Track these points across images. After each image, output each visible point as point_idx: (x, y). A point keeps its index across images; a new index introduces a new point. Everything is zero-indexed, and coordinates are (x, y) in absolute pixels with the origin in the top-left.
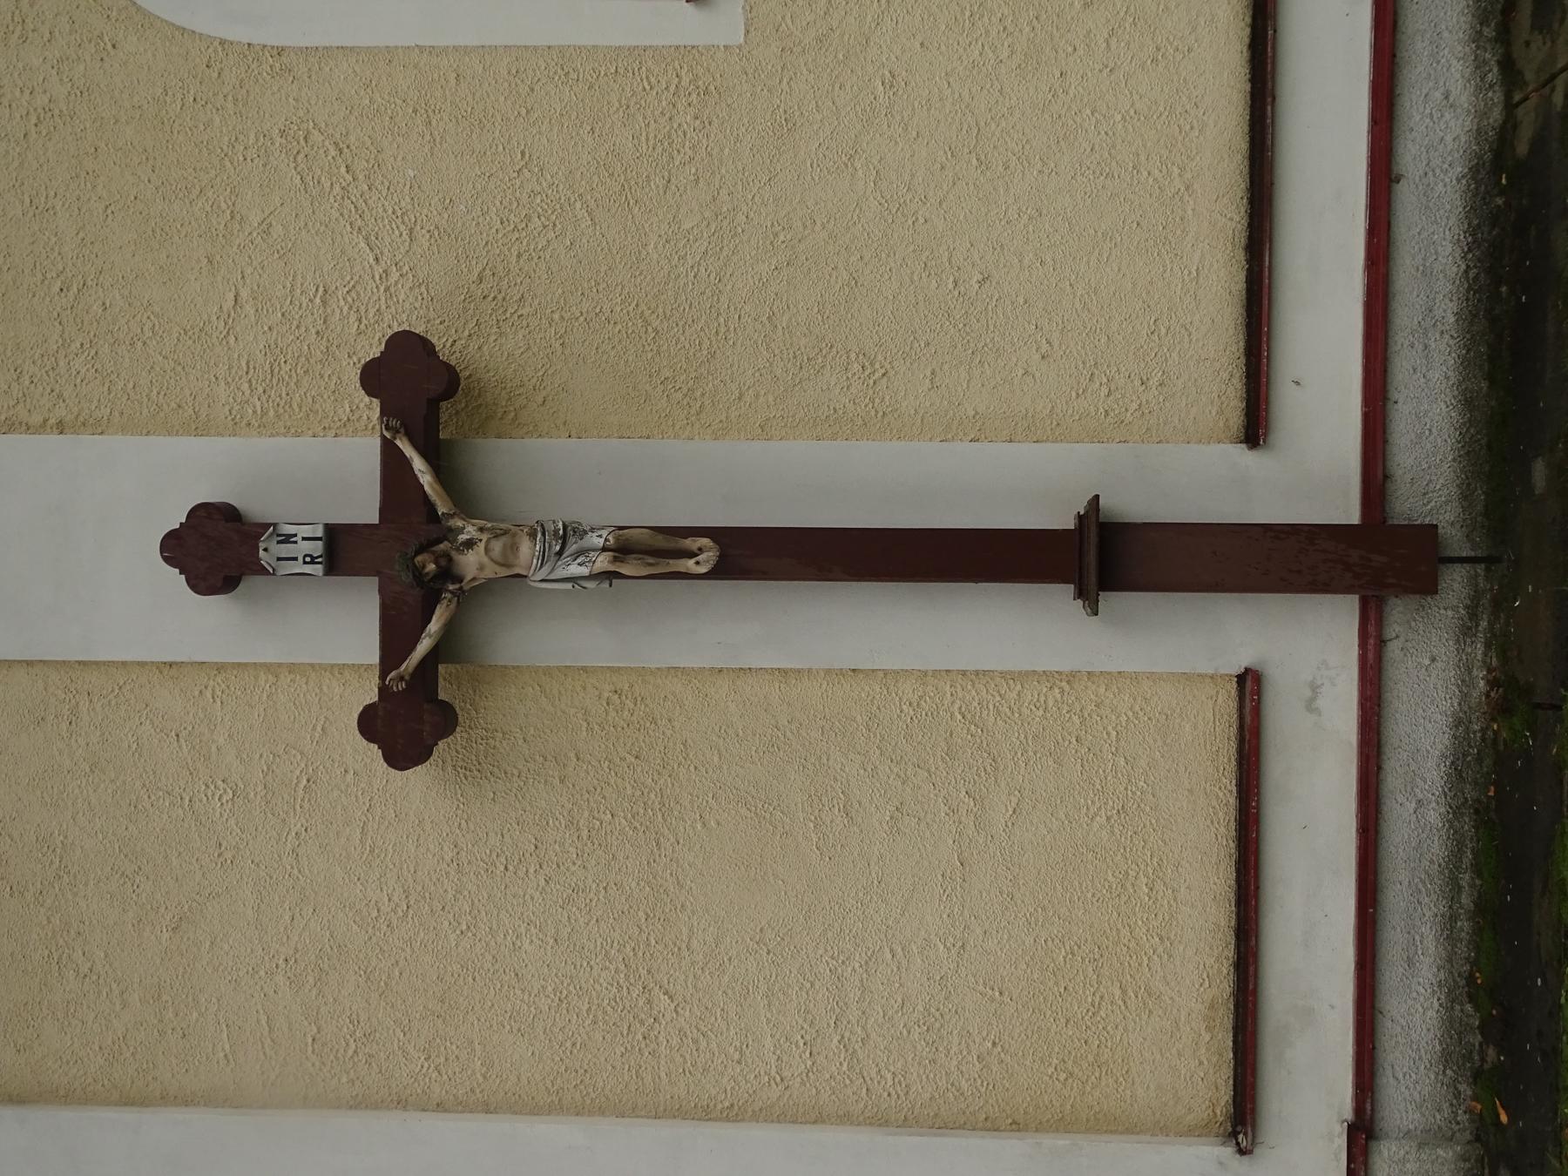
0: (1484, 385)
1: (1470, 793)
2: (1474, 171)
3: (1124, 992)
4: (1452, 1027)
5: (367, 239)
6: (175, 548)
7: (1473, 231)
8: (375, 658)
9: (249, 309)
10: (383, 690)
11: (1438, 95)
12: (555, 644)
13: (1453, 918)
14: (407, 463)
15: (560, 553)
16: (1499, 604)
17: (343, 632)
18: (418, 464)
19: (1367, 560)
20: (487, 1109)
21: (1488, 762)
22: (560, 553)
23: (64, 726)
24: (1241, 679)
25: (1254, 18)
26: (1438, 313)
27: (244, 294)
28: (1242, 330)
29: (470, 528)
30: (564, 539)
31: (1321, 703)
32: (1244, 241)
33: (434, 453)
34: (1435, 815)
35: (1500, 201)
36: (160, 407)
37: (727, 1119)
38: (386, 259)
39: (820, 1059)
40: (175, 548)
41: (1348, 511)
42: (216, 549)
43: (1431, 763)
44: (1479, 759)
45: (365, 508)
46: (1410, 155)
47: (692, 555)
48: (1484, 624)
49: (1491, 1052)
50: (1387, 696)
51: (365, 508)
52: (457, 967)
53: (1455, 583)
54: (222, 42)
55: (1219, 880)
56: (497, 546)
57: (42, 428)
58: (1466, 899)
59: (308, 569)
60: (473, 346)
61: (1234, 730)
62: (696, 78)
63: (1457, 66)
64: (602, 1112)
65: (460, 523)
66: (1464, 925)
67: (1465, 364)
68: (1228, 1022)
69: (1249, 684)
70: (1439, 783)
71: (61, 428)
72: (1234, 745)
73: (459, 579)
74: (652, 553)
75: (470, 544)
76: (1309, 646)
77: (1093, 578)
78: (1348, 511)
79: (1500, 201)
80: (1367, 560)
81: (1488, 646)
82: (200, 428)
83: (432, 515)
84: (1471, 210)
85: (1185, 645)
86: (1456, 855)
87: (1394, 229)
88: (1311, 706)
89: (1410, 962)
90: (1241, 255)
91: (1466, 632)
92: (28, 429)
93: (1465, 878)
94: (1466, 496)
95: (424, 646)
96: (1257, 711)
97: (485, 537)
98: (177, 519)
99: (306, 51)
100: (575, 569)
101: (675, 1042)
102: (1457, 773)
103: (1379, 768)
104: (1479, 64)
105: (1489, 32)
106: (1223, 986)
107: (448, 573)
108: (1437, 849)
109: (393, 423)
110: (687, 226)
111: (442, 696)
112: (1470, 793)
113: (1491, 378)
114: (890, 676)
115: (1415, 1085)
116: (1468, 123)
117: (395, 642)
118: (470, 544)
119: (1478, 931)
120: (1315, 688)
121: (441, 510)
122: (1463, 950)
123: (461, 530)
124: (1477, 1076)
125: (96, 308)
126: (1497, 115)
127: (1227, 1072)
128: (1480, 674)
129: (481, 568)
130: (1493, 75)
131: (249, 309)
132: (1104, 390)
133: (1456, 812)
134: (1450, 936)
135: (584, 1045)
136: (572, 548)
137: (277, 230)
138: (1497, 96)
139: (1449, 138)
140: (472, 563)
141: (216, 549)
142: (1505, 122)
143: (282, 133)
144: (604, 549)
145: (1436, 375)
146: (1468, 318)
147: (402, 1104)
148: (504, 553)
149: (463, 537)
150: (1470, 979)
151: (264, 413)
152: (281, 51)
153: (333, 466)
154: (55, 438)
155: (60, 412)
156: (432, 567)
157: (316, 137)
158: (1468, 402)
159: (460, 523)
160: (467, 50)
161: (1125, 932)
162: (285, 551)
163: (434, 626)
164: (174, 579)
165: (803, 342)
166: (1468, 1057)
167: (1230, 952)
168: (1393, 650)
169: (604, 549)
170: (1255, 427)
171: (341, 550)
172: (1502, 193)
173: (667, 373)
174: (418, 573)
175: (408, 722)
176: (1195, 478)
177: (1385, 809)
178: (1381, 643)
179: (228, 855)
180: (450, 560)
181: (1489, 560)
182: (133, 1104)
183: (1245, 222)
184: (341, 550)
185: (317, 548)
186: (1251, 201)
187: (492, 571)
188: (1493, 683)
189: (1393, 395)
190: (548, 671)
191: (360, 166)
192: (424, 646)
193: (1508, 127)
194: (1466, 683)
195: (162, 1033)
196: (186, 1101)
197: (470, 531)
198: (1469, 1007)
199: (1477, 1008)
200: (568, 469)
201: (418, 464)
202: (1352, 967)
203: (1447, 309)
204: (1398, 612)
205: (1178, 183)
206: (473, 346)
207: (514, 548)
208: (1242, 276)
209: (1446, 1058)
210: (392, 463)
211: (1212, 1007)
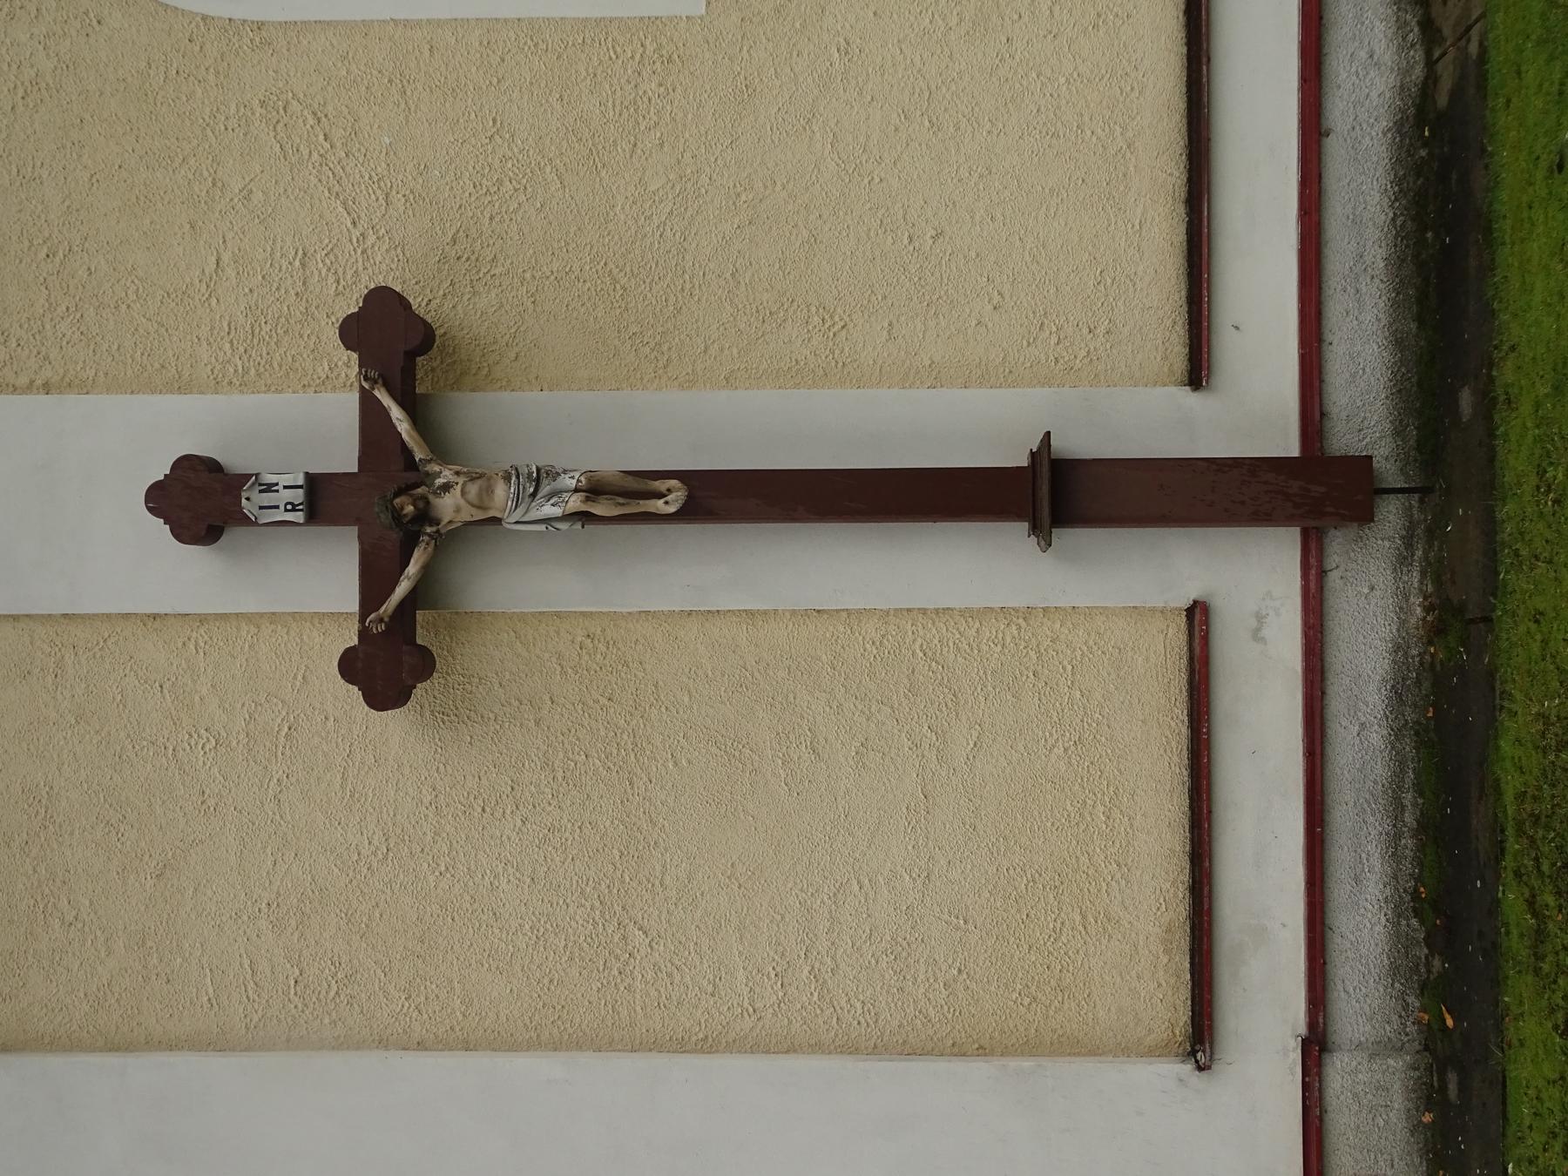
0: (1413, 326)
1: (1410, 715)
2: (1399, 126)
3: (1084, 917)
4: (1400, 942)
5: (344, 203)
6: (160, 499)
7: (1398, 181)
8: (354, 606)
11: (1363, 54)
12: (530, 589)
13: (1398, 837)
14: (385, 413)
15: (534, 495)
19: (1306, 492)
20: (467, 1046)
21: (1426, 685)
22: (534, 495)
23: (50, 679)
26: (1368, 259)
27: (226, 257)
28: (1183, 280)
29: (446, 473)
30: (538, 481)
31: (1265, 632)
32: (1184, 195)
34: (1377, 737)
35: (1423, 153)
36: (144, 368)
37: (702, 1051)
39: (791, 990)
41: (1289, 446)
42: (200, 501)
43: (1372, 687)
44: (1418, 682)
46: (1339, 110)
47: (660, 496)
48: (1419, 553)
51: (344, 457)
53: (1391, 513)
54: (204, 18)
56: (473, 489)
57: (29, 388)
58: (1409, 818)
60: (448, 305)
61: (1184, 661)
63: (1380, 27)
65: (437, 468)
66: (1408, 842)
67: (1395, 305)
68: (1185, 944)
69: (1198, 615)
70: (1381, 707)
71: (47, 388)
72: (1184, 676)
73: (436, 522)
74: (619, 500)
75: (447, 487)
76: (1253, 578)
78: (1282, 440)
79: (1423, 153)
80: (1306, 492)
81: (1423, 574)
82: (183, 386)
84: (1397, 162)
85: (1133, 579)
88: (1257, 635)
90: (1181, 210)
91: (1403, 561)
93: (1408, 798)
94: (1398, 432)
97: (461, 480)
98: (160, 471)
101: (650, 975)
102: (1397, 695)
104: (1401, 26)
106: (1179, 909)
107: (425, 515)
108: (1380, 770)
112: (1410, 715)
113: (1420, 320)
116: (1392, 80)
117: (374, 585)
118: (447, 487)
119: (1421, 848)
120: (1260, 618)
121: (418, 456)
122: (1407, 867)
125: (83, 273)
126: (1418, 72)
129: (458, 510)
131: (231, 273)
132: (1054, 339)
133: (1397, 734)
136: (545, 489)
137: (258, 196)
139: (1374, 94)
141: (200, 501)
143: (262, 103)
144: (576, 490)
145: (1368, 317)
146: (1396, 263)
148: (480, 495)
149: (440, 481)
150: (1415, 895)
151: (246, 371)
152: (260, 26)
155: (47, 373)
158: (1398, 342)
159: (437, 468)
160: (439, 23)
161: (1084, 859)
165: (766, 296)
166: (1415, 970)
167: (1185, 877)
168: (1334, 580)
169: (576, 490)
170: (1198, 370)
171: (322, 499)
172: (1425, 145)
174: (397, 515)
175: (388, 664)
176: (1148, 418)
178: (1322, 573)
180: (428, 503)
181: (1424, 491)
182: (118, 1049)
183: (1184, 178)
185: (298, 496)
186: (1190, 124)
189: (1328, 337)
190: (523, 617)
191: (337, 134)
194: (1403, 610)
195: (146, 979)
198: (1414, 922)
201: (396, 413)
203: (1377, 254)
206: (448, 305)
207: (489, 490)
209: (1394, 970)
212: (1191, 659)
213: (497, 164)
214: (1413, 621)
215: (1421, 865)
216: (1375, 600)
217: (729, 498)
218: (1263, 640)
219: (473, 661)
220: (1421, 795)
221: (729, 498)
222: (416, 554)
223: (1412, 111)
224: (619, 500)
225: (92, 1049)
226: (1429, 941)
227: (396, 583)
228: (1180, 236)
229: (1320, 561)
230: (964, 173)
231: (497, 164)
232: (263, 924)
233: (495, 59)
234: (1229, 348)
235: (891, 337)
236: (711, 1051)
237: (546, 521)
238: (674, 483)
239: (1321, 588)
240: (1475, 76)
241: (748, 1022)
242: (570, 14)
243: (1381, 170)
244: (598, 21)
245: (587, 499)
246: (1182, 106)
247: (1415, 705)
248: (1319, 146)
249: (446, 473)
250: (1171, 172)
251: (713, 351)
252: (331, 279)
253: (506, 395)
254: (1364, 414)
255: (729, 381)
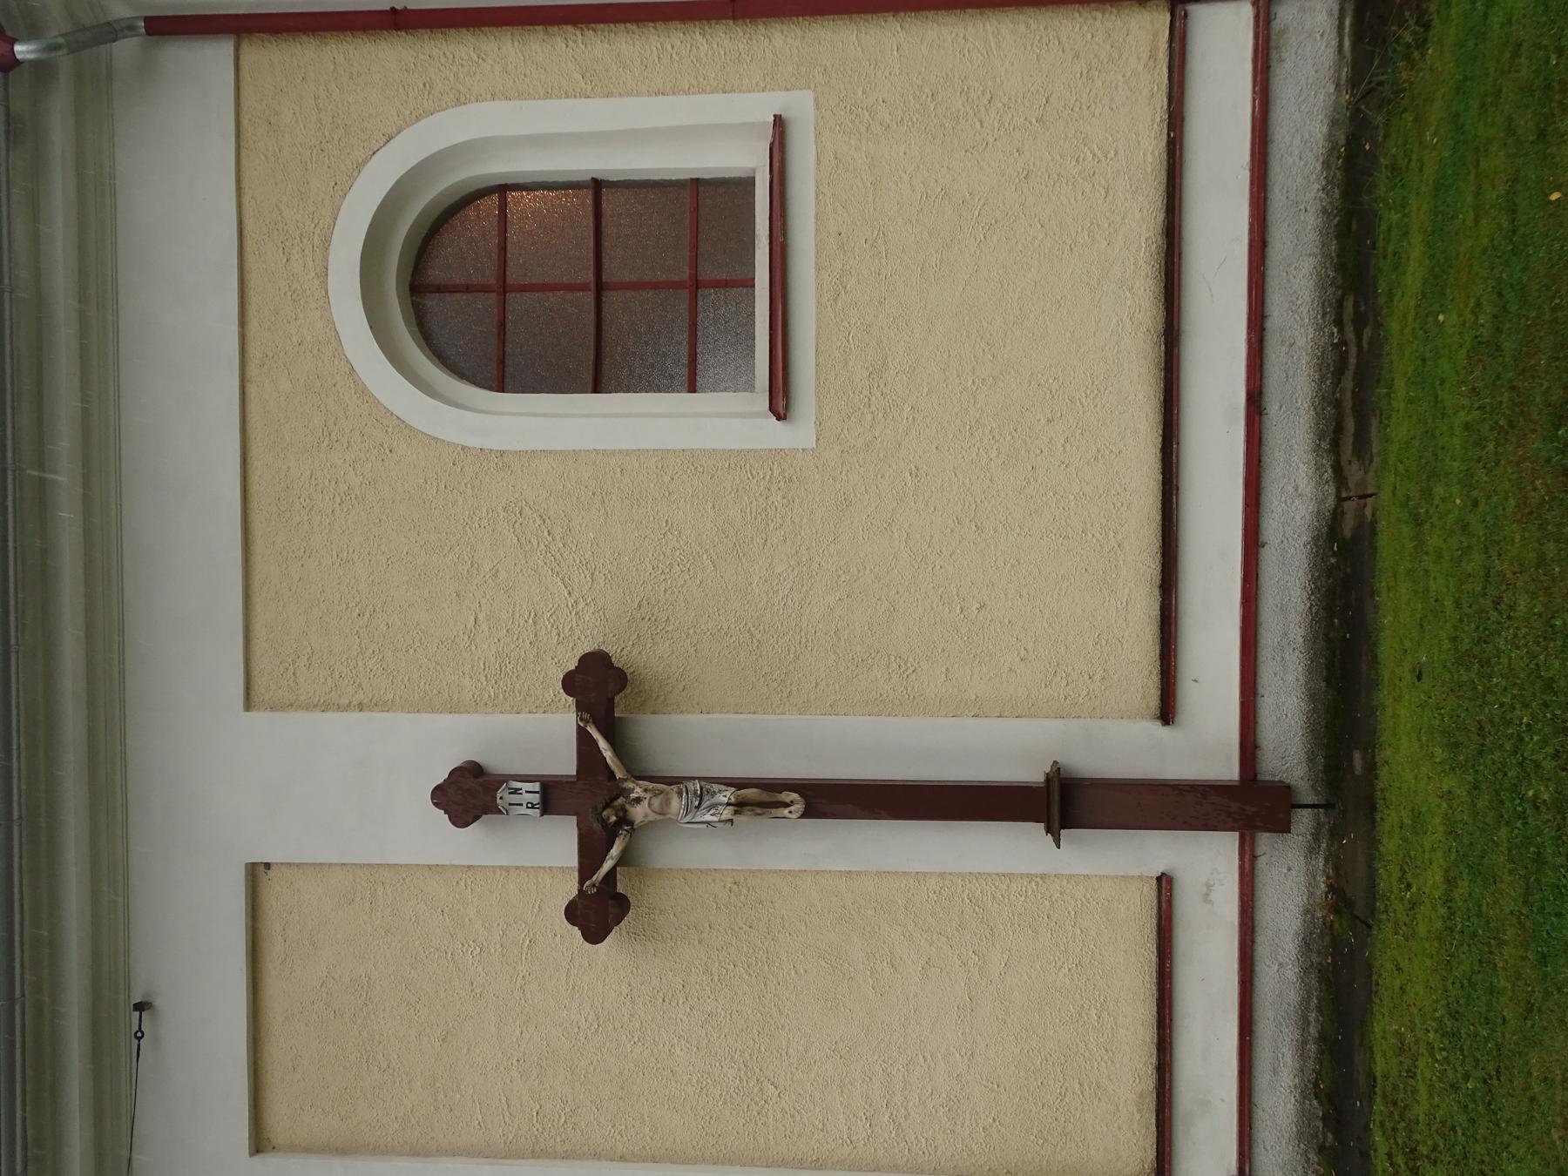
0: (1323, 685)
1: (1315, 959)
2: (1315, 539)
3: (1081, 1085)
4: (1304, 1115)
5: (563, 580)
6: (441, 796)
7: (1314, 580)
8: (573, 861)
9: (484, 627)
10: (580, 891)
11: (1290, 488)
12: (695, 854)
13: (1304, 1043)
14: (595, 742)
15: (698, 807)
16: (1335, 834)
17: (555, 846)
18: (602, 744)
19: (1243, 805)
20: (654, 1160)
21: (1327, 939)
22: (698, 807)
23: (367, 905)
24: (1159, 879)
25: (1164, 430)
26: (1291, 636)
27: (481, 617)
28: (1157, 641)
29: (638, 790)
30: (701, 797)
31: (1212, 896)
32: (1158, 582)
33: (613, 731)
34: (1291, 973)
35: (1333, 561)
36: (426, 694)
37: (815, 1168)
38: (576, 594)
39: (876, 1129)
40: (441, 796)
41: (1227, 769)
42: (469, 794)
43: (1288, 939)
44: (1321, 936)
45: (565, 764)
46: (1272, 528)
47: (787, 805)
48: (1324, 845)
49: (1330, 1137)
50: (1258, 893)
51: (565, 764)
52: (632, 1066)
53: (1303, 821)
54: (463, 448)
55: (1146, 1034)
56: (656, 802)
57: (347, 708)
58: (1313, 1030)
59: (530, 811)
60: (636, 651)
61: (1155, 911)
62: (784, 470)
63: (1303, 468)
64: (731, 1163)
65: (631, 785)
66: (1312, 1047)
67: (1311, 671)
68: (1153, 1107)
69: (1165, 883)
70: (1294, 952)
71: (361, 707)
72: (1155, 921)
73: (631, 823)
74: (760, 797)
75: (638, 800)
76: (1206, 862)
77: (1056, 824)
78: (1227, 769)
79: (1333, 561)
80: (1243, 805)
81: (1327, 860)
82: (454, 708)
83: (612, 775)
84: (1314, 566)
85: (1120, 860)
86: (1305, 1001)
87: (1261, 579)
88: (1206, 898)
89: (1275, 1071)
90: (1157, 592)
91: (1312, 850)
92: (339, 708)
93: (1312, 1016)
94: (1311, 760)
95: (607, 865)
96: (1170, 902)
97: (648, 796)
98: (441, 776)
99: (519, 454)
100: (708, 818)
101: (779, 1116)
102: (1306, 946)
103: (1253, 942)
104: (1319, 468)
105: (1325, 445)
106: (1149, 1083)
107: (624, 820)
108: (1293, 996)
109: (586, 716)
110: (779, 570)
111: (620, 889)
112: (1315, 959)
113: (1327, 680)
114: (920, 876)
115: (1280, 1102)
116: (1312, 507)
117: (587, 866)
118: (638, 800)
119: (1321, 1052)
120: (1209, 887)
121: (618, 776)
122: (1311, 1064)
123: (632, 791)
124: (1321, 1149)
125: (383, 627)
126: (1331, 502)
127: (1152, 1139)
128: (1321, 879)
129: (646, 816)
130: (1328, 474)
131: (484, 627)
132: (1064, 683)
133: (1305, 971)
134: (1302, 1056)
135: (718, 1118)
136: (706, 804)
137: (502, 574)
138: (1331, 489)
139: (1298, 518)
140: (639, 813)
141: (469, 794)
142: (1335, 510)
143: (505, 509)
144: (728, 804)
145: (1290, 678)
146: (1311, 641)
147: (597, 1156)
148: (661, 806)
149: (633, 796)
150: (1316, 1085)
151: (496, 697)
152: (502, 453)
153: (548, 737)
154: (357, 715)
155: (360, 697)
156: (614, 818)
157: (527, 511)
158: (1312, 696)
159: (631, 785)
160: (628, 453)
161: (1082, 1045)
162: (515, 798)
163: (615, 851)
164: (441, 816)
165: (859, 648)
166: (1315, 1136)
167: (1154, 1060)
168: (1262, 863)
169: (728, 804)
170: (1167, 712)
171: (553, 795)
172: (1334, 554)
173: (766, 669)
174: (604, 822)
175: (598, 911)
176: (1129, 748)
177: (1257, 969)
178: (1254, 858)
179: (478, 991)
180: (626, 811)
181: (1327, 806)
182: (418, 1155)
183: (1159, 569)
184: (553, 795)
185: (536, 798)
186: (1163, 555)
187: (652, 817)
188: (1331, 888)
189: (1261, 691)
190: (690, 871)
191: (557, 531)
192: (607, 865)
193: (1337, 516)
194: (1311, 885)
195: (437, 1109)
196: (454, 1153)
197: (638, 792)
198: (1315, 1102)
199: (1321, 1103)
200: (697, 735)
201: (602, 744)
202: (1236, 1073)
203: (1298, 633)
204: (1265, 841)
205: (1113, 542)
206: (636, 651)
207: (667, 802)
208: (1157, 606)
209: (1300, 1135)
210: (583, 738)
211: (1141, 1096)
212: (1160, 908)
213: (668, 553)
214: (1319, 893)
215: (1321, 1063)
216: (1291, 875)
217: (832, 800)
218: (1211, 902)
219: (651, 899)
220: (1322, 1014)
221: (832, 800)
222: (618, 842)
223: (1325, 530)
224: (760, 797)
225: (400, 1154)
226: (1324, 1119)
227: (600, 866)
228: (1155, 612)
229: (1253, 849)
230: (1000, 562)
231: (668, 553)
232: (514, 1073)
233: (667, 479)
234: (1190, 694)
235: (948, 679)
236: (820, 1169)
237: (708, 823)
238: (795, 796)
239: (1253, 868)
240: (1367, 531)
241: (847, 1150)
242: (719, 446)
243: (1301, 573)
244: (739, 452)
245: (736, 812)
246: (1159, 517)
247: (1319, 952)
248: (1257, 553)
249: (638, 790)
250: (1150, 566)
251: (821, 687)
252: (554, 633)
253: (675, 718)
254: (1287, 750)
255: (833, 710)
